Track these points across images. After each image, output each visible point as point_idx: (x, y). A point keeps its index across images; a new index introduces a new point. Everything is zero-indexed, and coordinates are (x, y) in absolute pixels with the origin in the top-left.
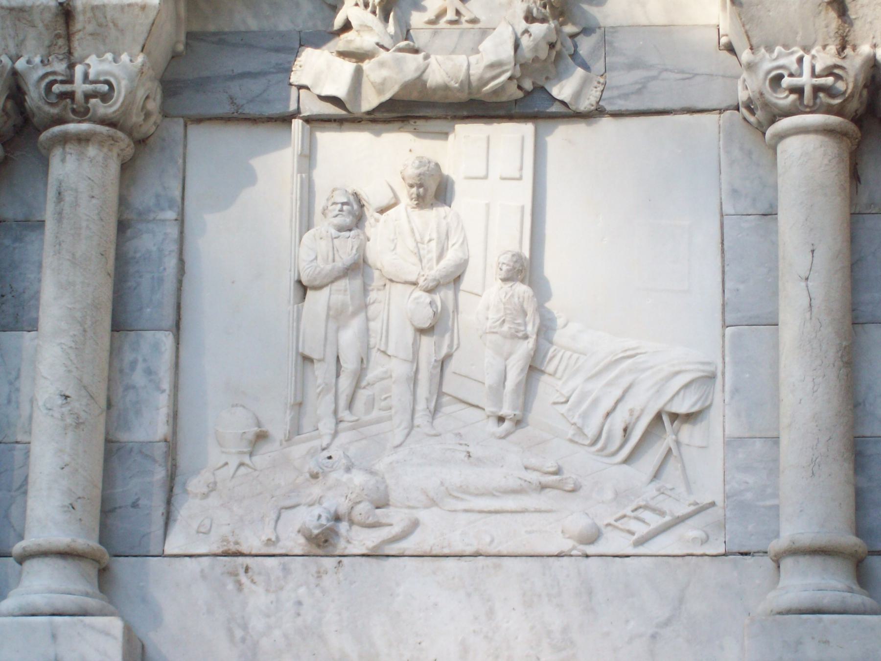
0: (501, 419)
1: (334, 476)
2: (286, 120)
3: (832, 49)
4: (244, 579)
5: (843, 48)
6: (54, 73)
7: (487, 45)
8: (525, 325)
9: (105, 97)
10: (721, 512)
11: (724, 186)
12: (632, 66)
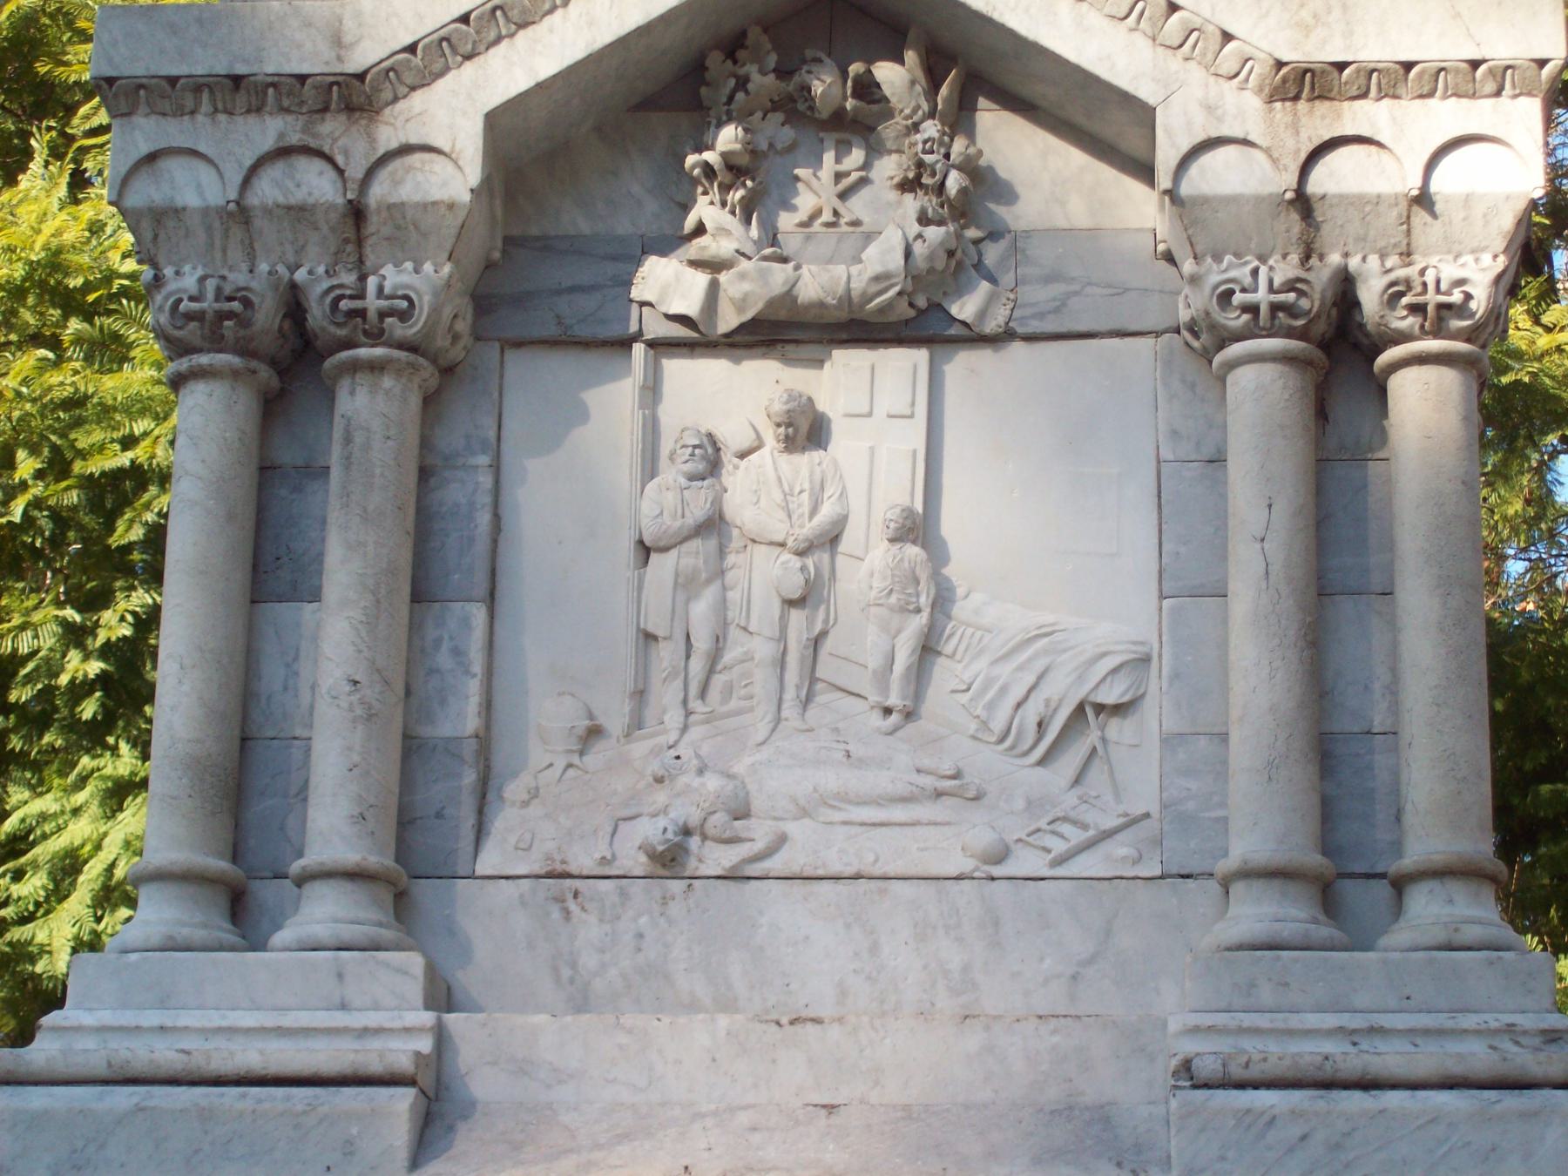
0: (888, 711)
2: (625, 344)
3: (1294, 258)
5: (1307, 257)
6: (341, 286)
7: (871, 252)
8: (918, 595)
9: (404, 316)
11: (1162, 427)
12: (1050, 279)
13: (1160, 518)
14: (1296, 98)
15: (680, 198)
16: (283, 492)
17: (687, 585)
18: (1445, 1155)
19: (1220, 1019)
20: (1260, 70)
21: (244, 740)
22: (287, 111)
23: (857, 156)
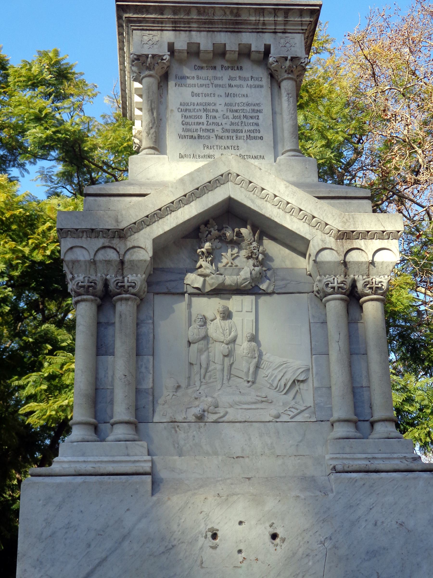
0: (248, 382)
1: (202, 399)
2: (183, 294)
3: (343, 276)
4: (177, 429)
5: (345, 276)
7: (242, 273)
8: (255, 354)
9: (133, 287)
10: (313, 409)
11: (310, 315)
12: (283, 280)
13: (311, 336)
14: (342, 239)
15: (195, 259)
16: (102, 329)
17: (200, 351)
18: (397, 488)
19: (338, 456)
20: (334, 232)
21: (96, 389)
22: (105, 237)
23: (236, 250)
